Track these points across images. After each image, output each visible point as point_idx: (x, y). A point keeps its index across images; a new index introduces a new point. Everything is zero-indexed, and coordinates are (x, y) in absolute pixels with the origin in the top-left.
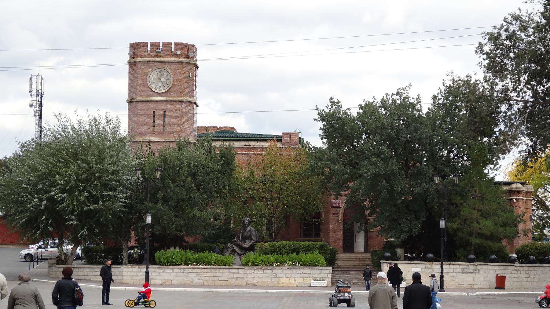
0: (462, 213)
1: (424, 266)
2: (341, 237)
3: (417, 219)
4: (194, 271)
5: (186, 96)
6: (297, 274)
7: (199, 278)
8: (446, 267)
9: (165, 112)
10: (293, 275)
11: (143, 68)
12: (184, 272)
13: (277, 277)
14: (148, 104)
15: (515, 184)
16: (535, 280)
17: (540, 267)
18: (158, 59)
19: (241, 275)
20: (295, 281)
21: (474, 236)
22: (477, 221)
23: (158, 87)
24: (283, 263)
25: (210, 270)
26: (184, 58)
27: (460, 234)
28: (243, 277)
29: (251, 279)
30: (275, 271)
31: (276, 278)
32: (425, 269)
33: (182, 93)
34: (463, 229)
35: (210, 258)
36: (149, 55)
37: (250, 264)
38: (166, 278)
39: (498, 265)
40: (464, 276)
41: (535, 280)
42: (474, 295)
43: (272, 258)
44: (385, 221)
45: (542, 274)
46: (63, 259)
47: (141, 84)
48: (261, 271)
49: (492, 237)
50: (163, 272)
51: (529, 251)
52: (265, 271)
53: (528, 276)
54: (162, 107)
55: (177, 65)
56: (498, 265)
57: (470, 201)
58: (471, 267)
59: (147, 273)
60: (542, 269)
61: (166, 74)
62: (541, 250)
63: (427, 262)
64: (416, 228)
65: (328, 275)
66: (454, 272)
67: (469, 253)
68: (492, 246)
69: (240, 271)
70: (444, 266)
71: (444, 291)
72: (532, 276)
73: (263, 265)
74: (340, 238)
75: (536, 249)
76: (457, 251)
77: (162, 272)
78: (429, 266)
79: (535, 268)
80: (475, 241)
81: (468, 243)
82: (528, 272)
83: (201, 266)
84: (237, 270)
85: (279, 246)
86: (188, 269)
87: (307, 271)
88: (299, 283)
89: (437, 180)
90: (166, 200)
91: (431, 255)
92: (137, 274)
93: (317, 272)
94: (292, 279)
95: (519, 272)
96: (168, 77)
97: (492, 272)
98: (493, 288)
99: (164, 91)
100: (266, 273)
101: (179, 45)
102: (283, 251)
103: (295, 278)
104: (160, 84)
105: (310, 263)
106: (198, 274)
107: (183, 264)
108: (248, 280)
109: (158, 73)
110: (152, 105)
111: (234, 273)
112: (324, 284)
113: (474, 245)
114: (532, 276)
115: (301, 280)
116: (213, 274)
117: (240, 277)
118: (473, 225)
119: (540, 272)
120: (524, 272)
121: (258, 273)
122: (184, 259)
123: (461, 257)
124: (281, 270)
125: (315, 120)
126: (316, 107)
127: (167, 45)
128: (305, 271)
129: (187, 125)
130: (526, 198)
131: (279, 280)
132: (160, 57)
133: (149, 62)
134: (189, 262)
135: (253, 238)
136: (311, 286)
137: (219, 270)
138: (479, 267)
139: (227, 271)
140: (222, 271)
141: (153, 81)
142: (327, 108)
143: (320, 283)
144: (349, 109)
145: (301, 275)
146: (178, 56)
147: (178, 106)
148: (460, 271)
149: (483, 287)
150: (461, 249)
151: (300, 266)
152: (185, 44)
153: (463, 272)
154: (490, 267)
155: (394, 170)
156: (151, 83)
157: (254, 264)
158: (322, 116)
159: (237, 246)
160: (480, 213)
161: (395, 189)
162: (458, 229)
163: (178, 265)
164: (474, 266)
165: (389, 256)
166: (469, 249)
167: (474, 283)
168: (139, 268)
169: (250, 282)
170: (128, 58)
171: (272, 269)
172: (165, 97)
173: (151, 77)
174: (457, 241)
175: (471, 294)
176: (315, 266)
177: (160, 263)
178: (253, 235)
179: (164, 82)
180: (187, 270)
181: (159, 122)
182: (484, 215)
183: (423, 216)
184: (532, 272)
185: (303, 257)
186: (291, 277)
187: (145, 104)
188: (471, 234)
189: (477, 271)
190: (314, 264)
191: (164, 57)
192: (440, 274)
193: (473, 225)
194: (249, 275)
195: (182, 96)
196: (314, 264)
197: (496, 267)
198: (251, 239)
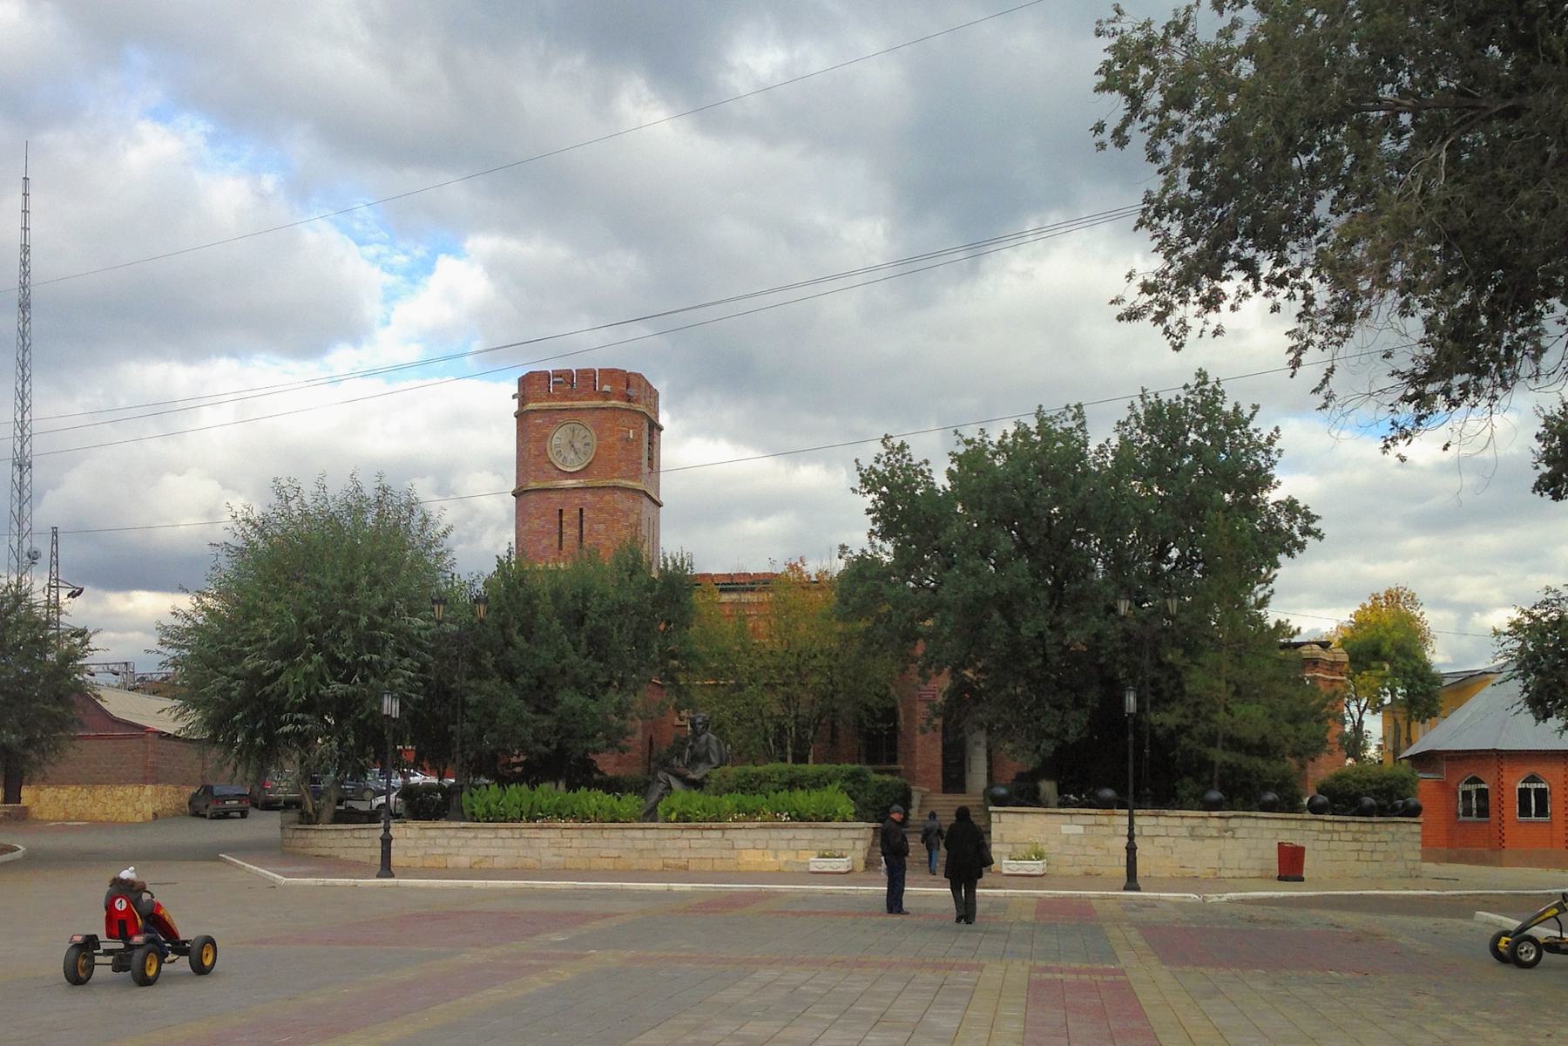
0: (1187, 688)
1: (1091, 820)
2: (939, 763)
3: (1079, 704)
4: (543, 834)
5: (623, 478)
6: (783, 840)
7: (555, 851)
8: (1146, 822)
9: (581, 510)
10: (772, 844)
11: (540, 424)
12: (521, 838)
13: (733, 848)
14: (550, 495)
15: (1307, 647)
16: (1376, 856)
17: (1389, 825)
19: (650, 845)
20: (776, 857)
21: (1219, 745)
22: (1226, 706)
24: (751, 814)
25: (579, 831)
27: (1184, 741)
29: (675, 854)
30: (729, 834)
33: (614, 470)
34: (1191, 727)
35: (584, 802)
36: (550, 397)
37: (674, 816)
38: (482, 852)
39: (1282, 819)
40: (1197, 845)
41: (1376, 856)
42: (1223, 899)
43: (728, 802)
44: (1004, 712)
45: (1393, 841)
46: (310, 811)
47: (536, 455)
48: (695, 834)
49: (1263, 749)
50: (475, 838)
51: (1354, 788)
52: (706, 833)
53: (1357, 846)
56: (1282, 819)
57: (1209, 658)
58: (1213, 822)
59: (386, 842)
60: (1392, 828)
61: (583, 432)
62: (1381, 784)
63: (1098, 811)
64: (1076, 725)
66: (1168, 835)
67: (1209, 786)
68: (1264, 771)
69: (649, 834)
70: (1137, 821)
71: (1138, 889)
72: (1367, 847)
73: (705, 820)
75: (1370, 781)
76: (1177, 784)
77: (470, 839)
78: (1105, 820)
79: (1377, 826)
80: (1219, 755)
81: (1206, 765)
82: (1358, 836)
83: (562, 824)
84: (641, 831)
85: (757, 776)
86: (529, 831)
87: (804, 834)
88: (787, 862)
89: (1123, 607)
90: (510, 675)
91: (1108, 793)
92: (416, 842)
93: (826, 835)
94: (770, 853)
95: (1336, 836)
97: (1268, 835)
98: (1271, 878)
99: (579, 468)
100: (708, 839)
101: (611, 374)
102: (765, 786)
103: (776, 851)
104: (572, 455)
105: (813, 814)
106: (552, 841)
107: (524, 818)
108: (667, 855)
109: (568, 431)
110: (556, 497)
111: (634, 839)
112: (841, 865)
113: (1220, 768)
114: (1367, 847)
115: (790, 856)
116: (586, 843)
117: (647, 850)
118: (1215, 717)
119: (1385, 836)
120: (1349, 837)
121: (689, 839)
122: (527, 807)
123: (1187, 799)
124: (743, 831)
125: (854, 490)
126: (856, 461)
127: (587, 375)
128: (799, 834)
130: (1331, 677)
132: (572, 400)
133: (548, 410)
134: (540, 814)
135: (713, 759)
136: (811, 870)
137: (600, 831)
138: (1233, 823)
139: (619, 834)
140: (606, 834)
142: (878, 461)
143: (832, 864)
144: (927, 462)
145: (792, 843)
146: (606, 396)
147: (607, 498)
148: (1185, 832)
149: (1244, 873)
150: (1187, 780)
151: (792, 820)
153: (1193, 836)
154: (1262, 823)
155: (1018, 585)
157: (684, 818)
158: (869, 481)
159: (678, 776)
160: (1233, 688)
161: (1023, 630)
162: (1181, 729)
163: (513, 820)
164: (1222, 820)
165: (1003, 795)
166: (1207, 778)
167: (1221, 865)
168: (421, 829)
169: (671, 861)
170: (514, 405)
171: (723, 829)
174: (1178, 760)
175: (1213, 898)
176: (827, 820)
177: (473, 817)
180: (527, 833)
181: (570, 532)
182: (1239, 692)
183: (1093, 696)
184: (1369, 837)
185: (800, 798)
186: (767, 848)
187: (543, 495)
188: (1211, 740)
189: (1230, 833)
190: (825, 816)
191: (579, 400)
192: (1126, 840)
193: (1215, 717)
194: (668, 844)
195: (614, 477)
196: (823, 817)
197: (1279, 824)
198: (710, 762)
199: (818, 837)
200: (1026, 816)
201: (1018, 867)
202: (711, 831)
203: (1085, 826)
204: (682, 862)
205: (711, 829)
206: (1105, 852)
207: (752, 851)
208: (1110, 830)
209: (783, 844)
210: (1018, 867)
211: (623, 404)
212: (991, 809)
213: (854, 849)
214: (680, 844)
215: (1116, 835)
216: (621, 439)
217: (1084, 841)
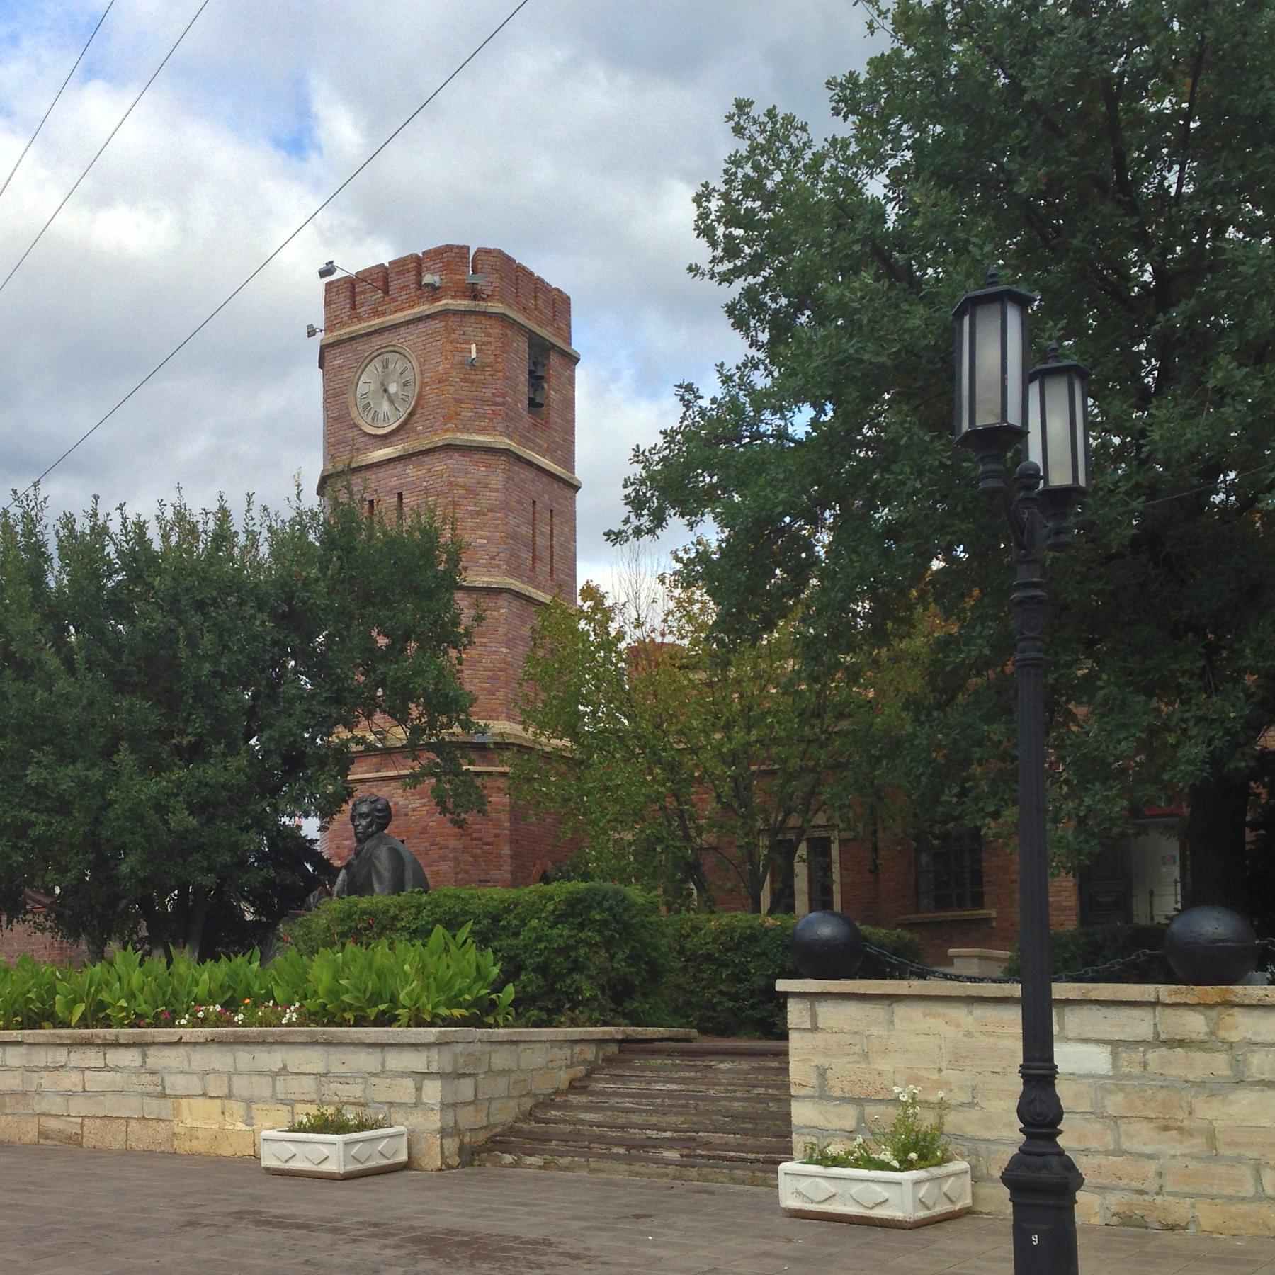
1: (1139, 1025)
6: (260, 1073)
9: (400, 495)
13: (163, 1095)
18: (376, 322)
23: (381, 416)
26: (453, 297)
28: (24, 1094)
30: (157, 1058)
31: (162, 1101)
32: (1154, 1056)
48: (91, 1057)
54: (394, 482)
55: (436, 325)
61: (400, 366)
63: (1165, 992)
65: (419, 1089)
74: (1065, 904)
78: (1195, 1024)
94: (238, 1108)
96: (408, 376)
100: (117, 1069)
103: (249, 1102)
104: (386, 407)
121: (83, 1070)
124: (182, 1050)
129: (472, 529)
131: (177, 1110)
141: (366, 401)
145: (280, 1082)
152: (458, 247)
156: (361, 409)
165: (826, 942)
172: (400, 447)
173: (362, 389)
178: (378, 873)
179: (396, 394)
186: (230, 1096)
195: (448, 430)
199: (337, 1068)
200: (901, 1010)
201: (830, 1187)
202: (122, 1051)
203: (1116, 1045)
204: (71, 1127)
205: (116, 1044)
206: (1197, 1144)
207: (200, 1101)
208: (1219, 1064)
209: (262, 1087)
210: (830, 1187)
211: (463, 304)
212: (782, 985)
213: (418, 1104)
214: (71, 1080)
215: (1240, 1082)
216: (462, 363)
217: (1114, 1104)
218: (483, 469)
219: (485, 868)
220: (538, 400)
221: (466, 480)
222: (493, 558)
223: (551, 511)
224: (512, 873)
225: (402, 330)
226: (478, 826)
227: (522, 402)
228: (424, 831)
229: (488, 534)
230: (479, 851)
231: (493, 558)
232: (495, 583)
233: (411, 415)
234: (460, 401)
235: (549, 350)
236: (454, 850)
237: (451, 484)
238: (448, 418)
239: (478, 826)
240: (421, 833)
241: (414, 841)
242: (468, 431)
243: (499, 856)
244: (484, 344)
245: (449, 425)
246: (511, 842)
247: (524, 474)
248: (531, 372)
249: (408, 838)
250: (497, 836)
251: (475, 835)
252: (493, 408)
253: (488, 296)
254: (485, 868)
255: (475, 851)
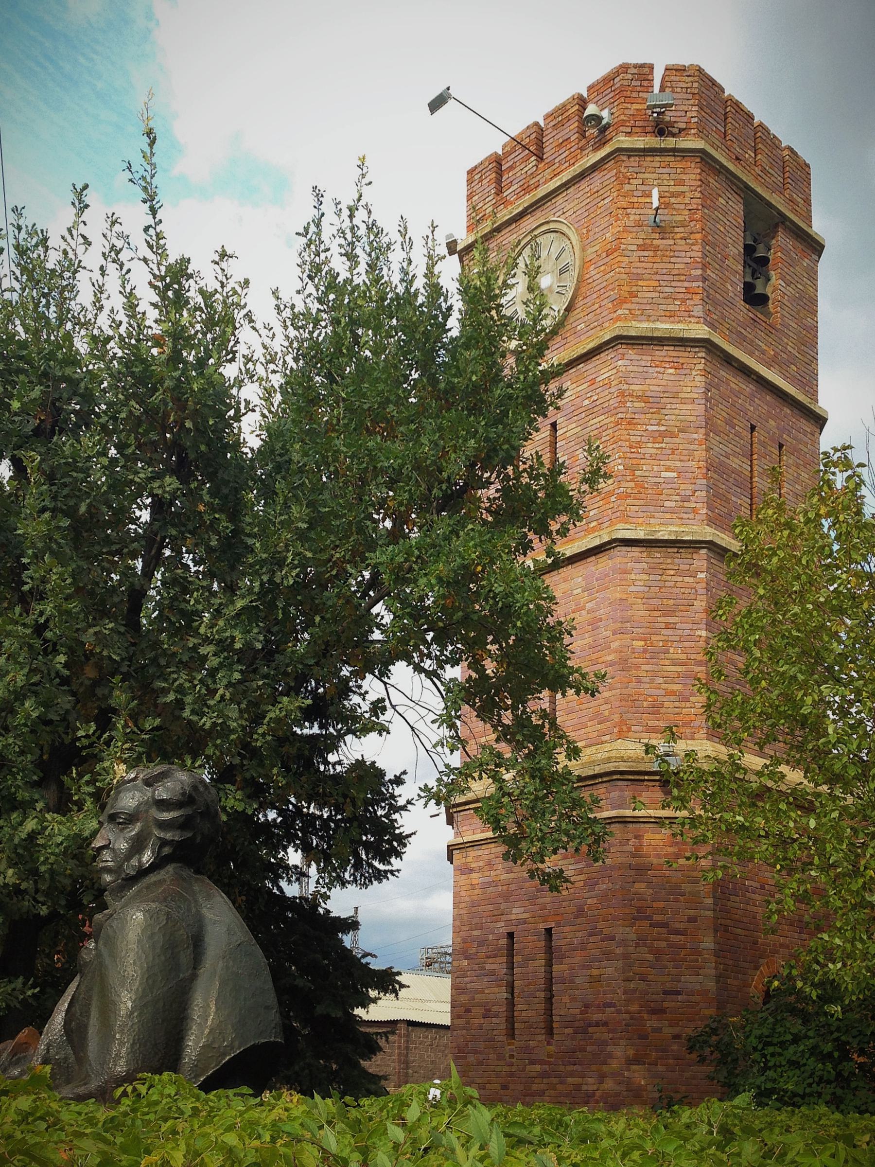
96: (566, 258)
129: (653, 457)
152: (636, 66)
179: (550, 288)
195: (618, 319)
218: (671, 371)
219: (674, 971)
220: (759, 290)
221: (645, 387)
222: (685, 499)
223: (781, 446)
224: (719, 978)
225: (560, 200)
226: (661, 904)
227: (733, 284)
228: (580, 912)
229: (678, 464)
230: (663, 944)
231: (685, 499)
232: (688, 533)
233: (568, 309)
234: (639, 277)
235: (776, 226)
236: (624, 943)
237: (622, 394)
238: (620, 302)
239: (661, 904)
240: (577, 917)
241: (567, 929)
242: (649, 318)
243: (697, 952)
244: (673, 195)
245: (620, 312)
246: (716, 931)
247: (737, 383)
248: (749, 250)
249: (558, 925)
250: (692, 920)
251: (656, 917)
252: (686, 284)
253: (681, 130)
254: (674, 971)
255: (656, 944)
